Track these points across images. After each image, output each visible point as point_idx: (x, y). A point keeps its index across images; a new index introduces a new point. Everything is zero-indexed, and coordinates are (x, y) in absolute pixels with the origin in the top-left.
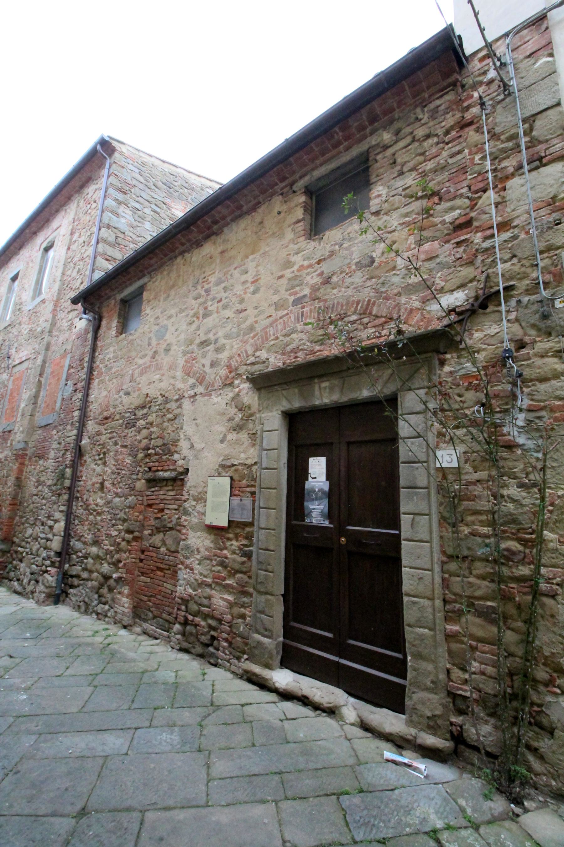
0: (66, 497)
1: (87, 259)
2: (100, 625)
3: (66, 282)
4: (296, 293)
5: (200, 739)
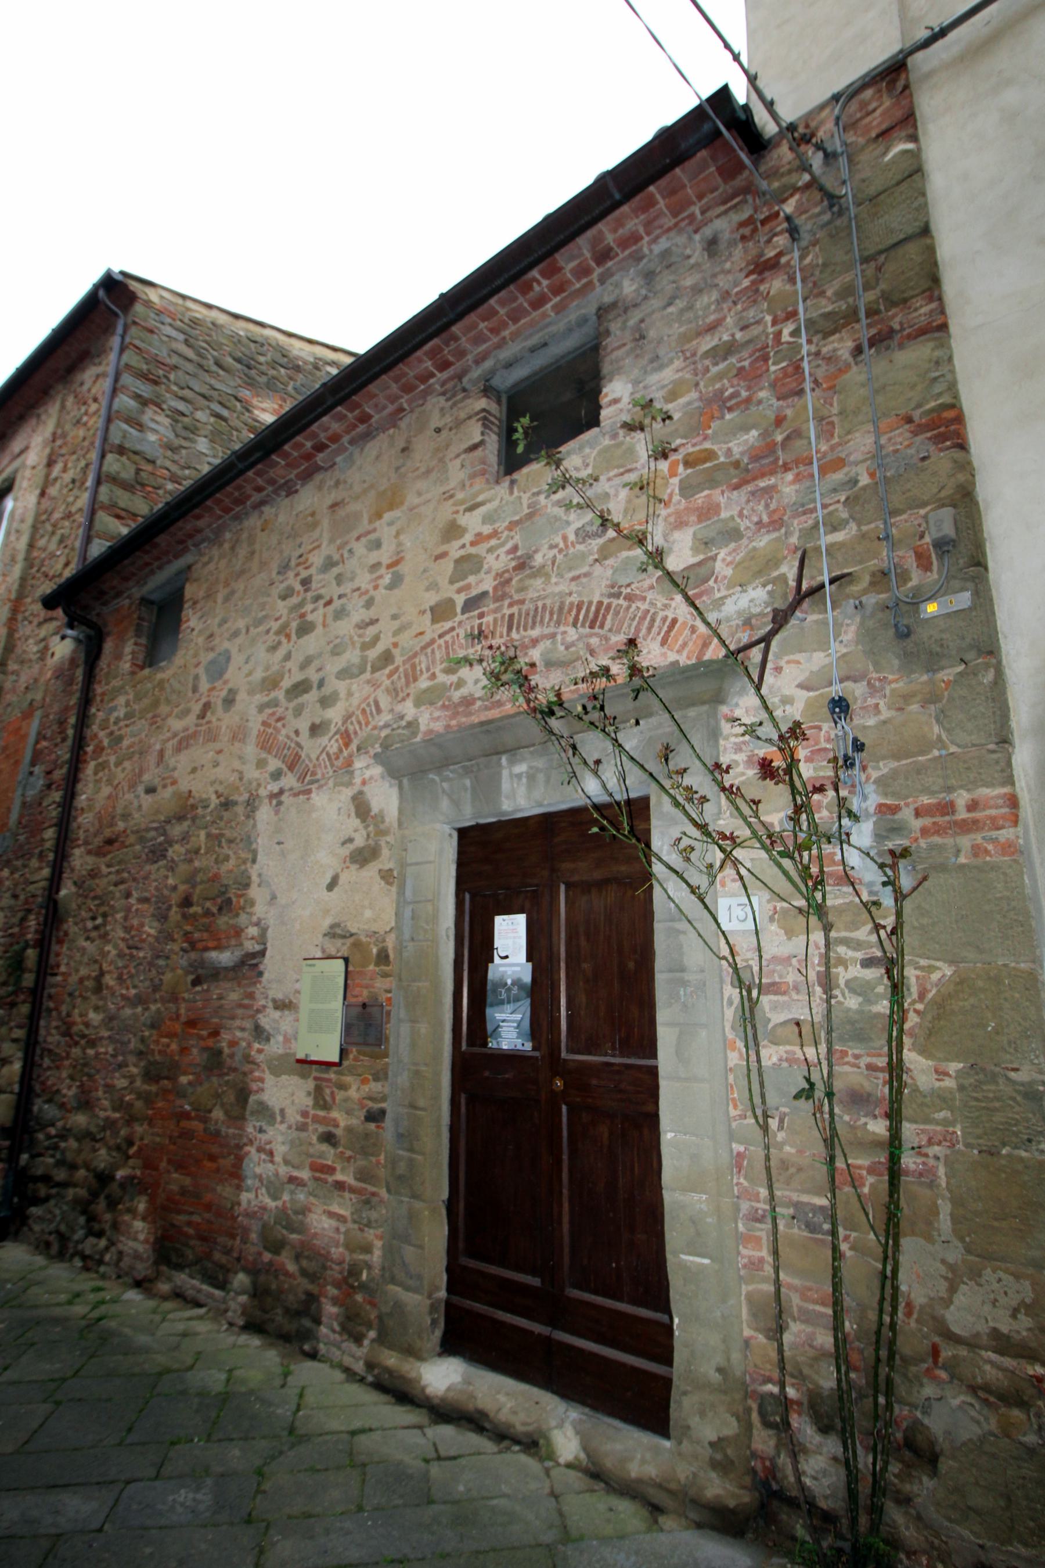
0: (25, 1009)
1: (77, 516)
2: (86, 1283)
3: (37, 562)
4: (468, 587)
5: (254, 1498)
